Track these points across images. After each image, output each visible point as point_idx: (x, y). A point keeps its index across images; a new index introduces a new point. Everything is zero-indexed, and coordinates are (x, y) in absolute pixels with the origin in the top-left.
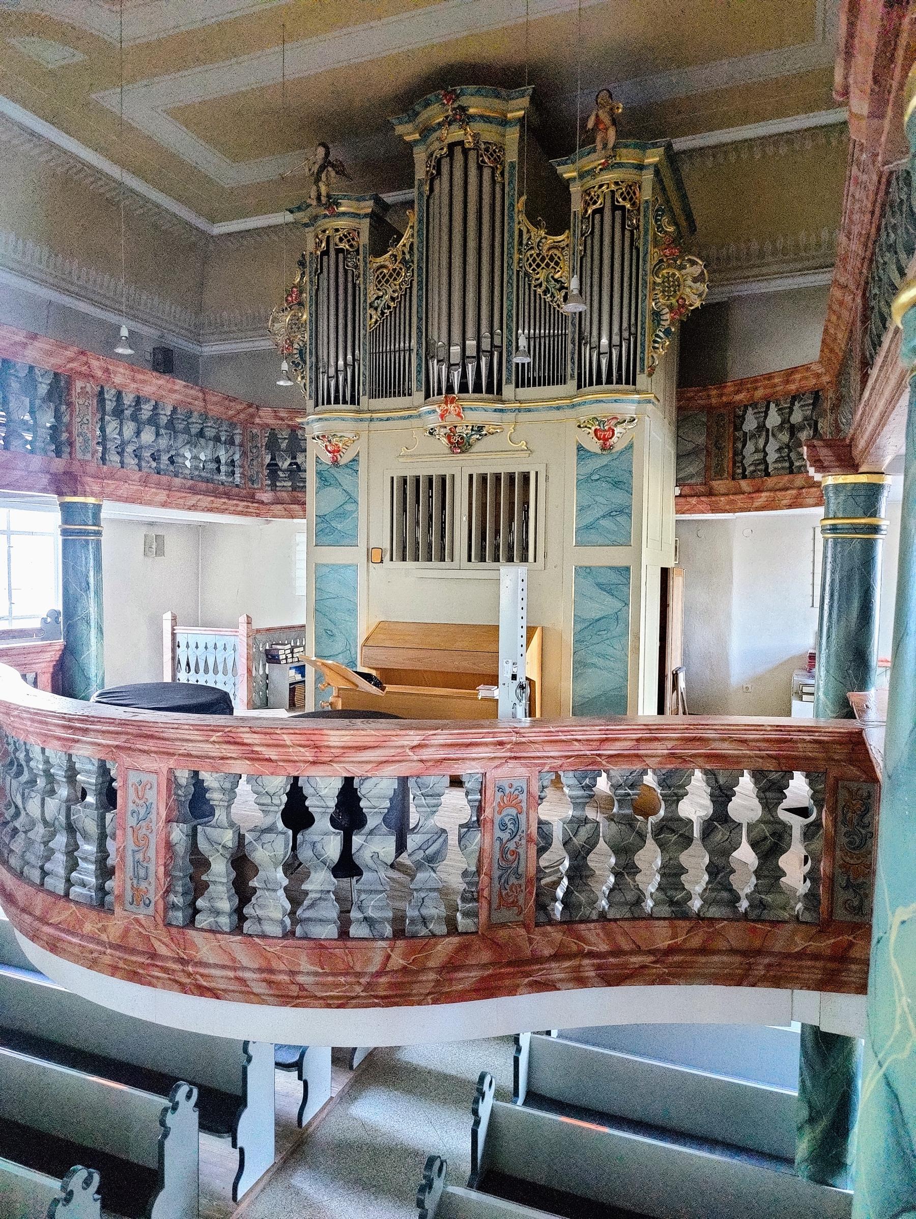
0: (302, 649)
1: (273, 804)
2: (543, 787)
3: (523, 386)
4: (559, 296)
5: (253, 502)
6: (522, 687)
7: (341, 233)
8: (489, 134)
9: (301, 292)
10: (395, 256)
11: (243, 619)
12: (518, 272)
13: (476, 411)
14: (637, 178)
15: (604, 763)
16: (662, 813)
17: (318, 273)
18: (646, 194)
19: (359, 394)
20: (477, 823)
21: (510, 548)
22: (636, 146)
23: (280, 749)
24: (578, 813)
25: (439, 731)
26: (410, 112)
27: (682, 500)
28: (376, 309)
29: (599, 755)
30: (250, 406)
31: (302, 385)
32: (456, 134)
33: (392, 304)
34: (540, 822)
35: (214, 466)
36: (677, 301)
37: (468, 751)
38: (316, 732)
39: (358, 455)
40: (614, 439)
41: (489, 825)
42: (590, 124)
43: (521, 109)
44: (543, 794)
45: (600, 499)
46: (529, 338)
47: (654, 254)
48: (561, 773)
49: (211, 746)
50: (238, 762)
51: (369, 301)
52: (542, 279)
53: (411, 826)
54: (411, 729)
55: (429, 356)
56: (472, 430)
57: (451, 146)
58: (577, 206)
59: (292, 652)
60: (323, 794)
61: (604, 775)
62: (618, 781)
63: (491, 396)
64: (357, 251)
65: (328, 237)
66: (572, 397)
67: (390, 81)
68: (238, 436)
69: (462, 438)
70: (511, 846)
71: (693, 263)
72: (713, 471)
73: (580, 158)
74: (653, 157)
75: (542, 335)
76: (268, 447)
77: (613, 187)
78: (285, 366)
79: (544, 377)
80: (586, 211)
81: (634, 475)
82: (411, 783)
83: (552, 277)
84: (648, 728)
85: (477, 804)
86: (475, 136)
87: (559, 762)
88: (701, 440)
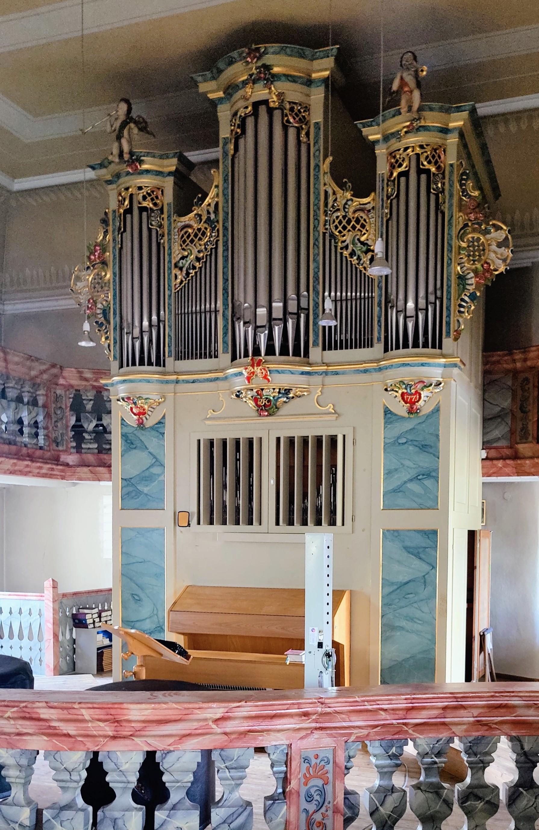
0: (109, 613)
1: (72, 781)
2: (350, 758)
3: (330, 349)
4: (366, 259)
5: (57, 465)
6: (328, 655)
7: (144, 192)
8: (294, 93)
9: (104, 250)
10: (200, 216)
11: (48, 584)
12: (324, 234)
13: (284, 374)
14: (440, 141)
15: (410, 731)
16: (468, 780)
17: (122, 231)
18: (451, 158)
19: (164, 356)
20: (283, 795)
21: (318, 511)
22: (441, 110)
23: (79, 725)
24: (385, 783)
25: (243, 703)
26: (215, 71)
27: (488, 463)
28: (181, 269)
29: (405, 724)
30: (53, 366)
31: (106, 345)
32: (260, 92)
33: (197, 265)
34: (347, 793)
35: (17, 427)
36: (482, 266)
37: (273, 723)
38: (116, 706)
39: (164, 417)
40: (421, 403)
41: (294, 796)
42: (395, 86)
43: (326, 70)
44: (349, 765)
45: (407, 463)
46: (335, 301)
47: (459, 218)
48: (368, 742)
49: (5, 722)
50: (34, 738)
51: (173, 262)
52: (348, 241)
53: (217, 799)
54: (214, 701)
55: (235, 316)
56: (279, 393)
57: (256, 105)
58: (382, 168)
59: (100, 617)
60: (124, 768)
61: (411, 743)
62: (425, 749)
63: (297, 359)
64: (162, 210)
65: (131, 196)
66: (378, 361)
67: (194, 37)
68: (42, 397)
69: (269, 401)
70: (318, 817)
71: (498, 228)
72: (518, 435)
73: (383, 121)
74: (458, 121)
75: (349, 298)
76: (72, 408)
77: (418, 150)
78: (86, 327)
79: (351, 339)
80: (392, 174)
81: (440, 437)
82: (215, 756)
83: (359, 239)
84: (454, 696)
85: (282, 775)
86: (280, 95)
87: (365, 732)
88: (507, 403)
